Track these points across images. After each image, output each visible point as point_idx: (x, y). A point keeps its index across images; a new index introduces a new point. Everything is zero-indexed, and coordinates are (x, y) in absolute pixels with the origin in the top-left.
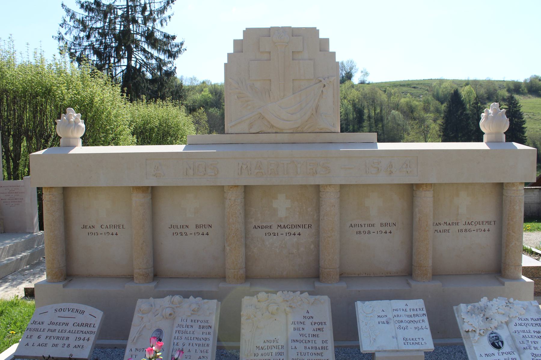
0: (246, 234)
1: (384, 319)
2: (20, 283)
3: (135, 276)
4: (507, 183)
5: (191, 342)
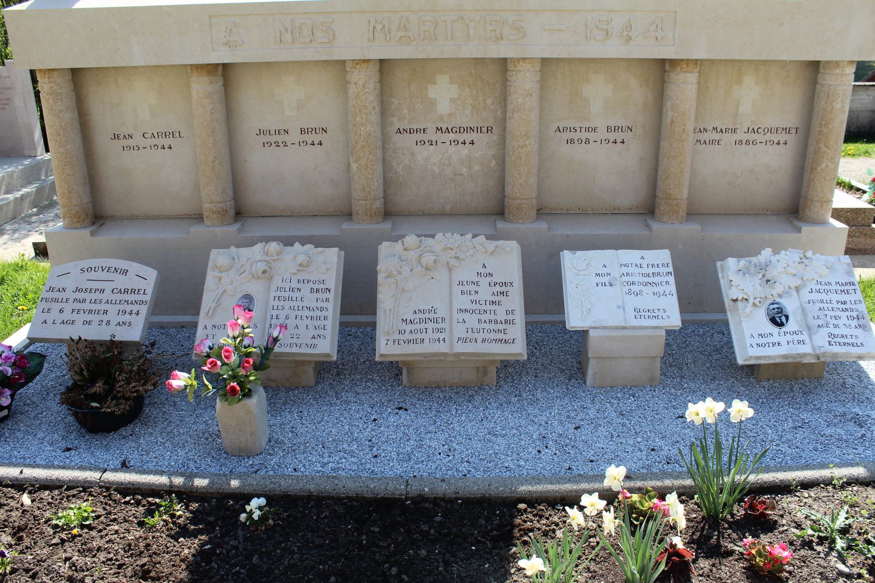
0: (383, 143)
1: (606, 280)
2: (26, 236)
3: (206, 214)
4: (828, 62)
5: (299, 313)
